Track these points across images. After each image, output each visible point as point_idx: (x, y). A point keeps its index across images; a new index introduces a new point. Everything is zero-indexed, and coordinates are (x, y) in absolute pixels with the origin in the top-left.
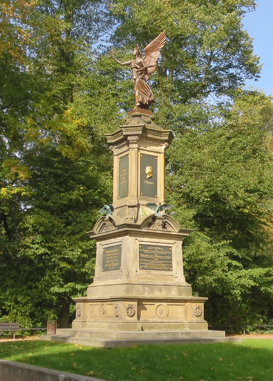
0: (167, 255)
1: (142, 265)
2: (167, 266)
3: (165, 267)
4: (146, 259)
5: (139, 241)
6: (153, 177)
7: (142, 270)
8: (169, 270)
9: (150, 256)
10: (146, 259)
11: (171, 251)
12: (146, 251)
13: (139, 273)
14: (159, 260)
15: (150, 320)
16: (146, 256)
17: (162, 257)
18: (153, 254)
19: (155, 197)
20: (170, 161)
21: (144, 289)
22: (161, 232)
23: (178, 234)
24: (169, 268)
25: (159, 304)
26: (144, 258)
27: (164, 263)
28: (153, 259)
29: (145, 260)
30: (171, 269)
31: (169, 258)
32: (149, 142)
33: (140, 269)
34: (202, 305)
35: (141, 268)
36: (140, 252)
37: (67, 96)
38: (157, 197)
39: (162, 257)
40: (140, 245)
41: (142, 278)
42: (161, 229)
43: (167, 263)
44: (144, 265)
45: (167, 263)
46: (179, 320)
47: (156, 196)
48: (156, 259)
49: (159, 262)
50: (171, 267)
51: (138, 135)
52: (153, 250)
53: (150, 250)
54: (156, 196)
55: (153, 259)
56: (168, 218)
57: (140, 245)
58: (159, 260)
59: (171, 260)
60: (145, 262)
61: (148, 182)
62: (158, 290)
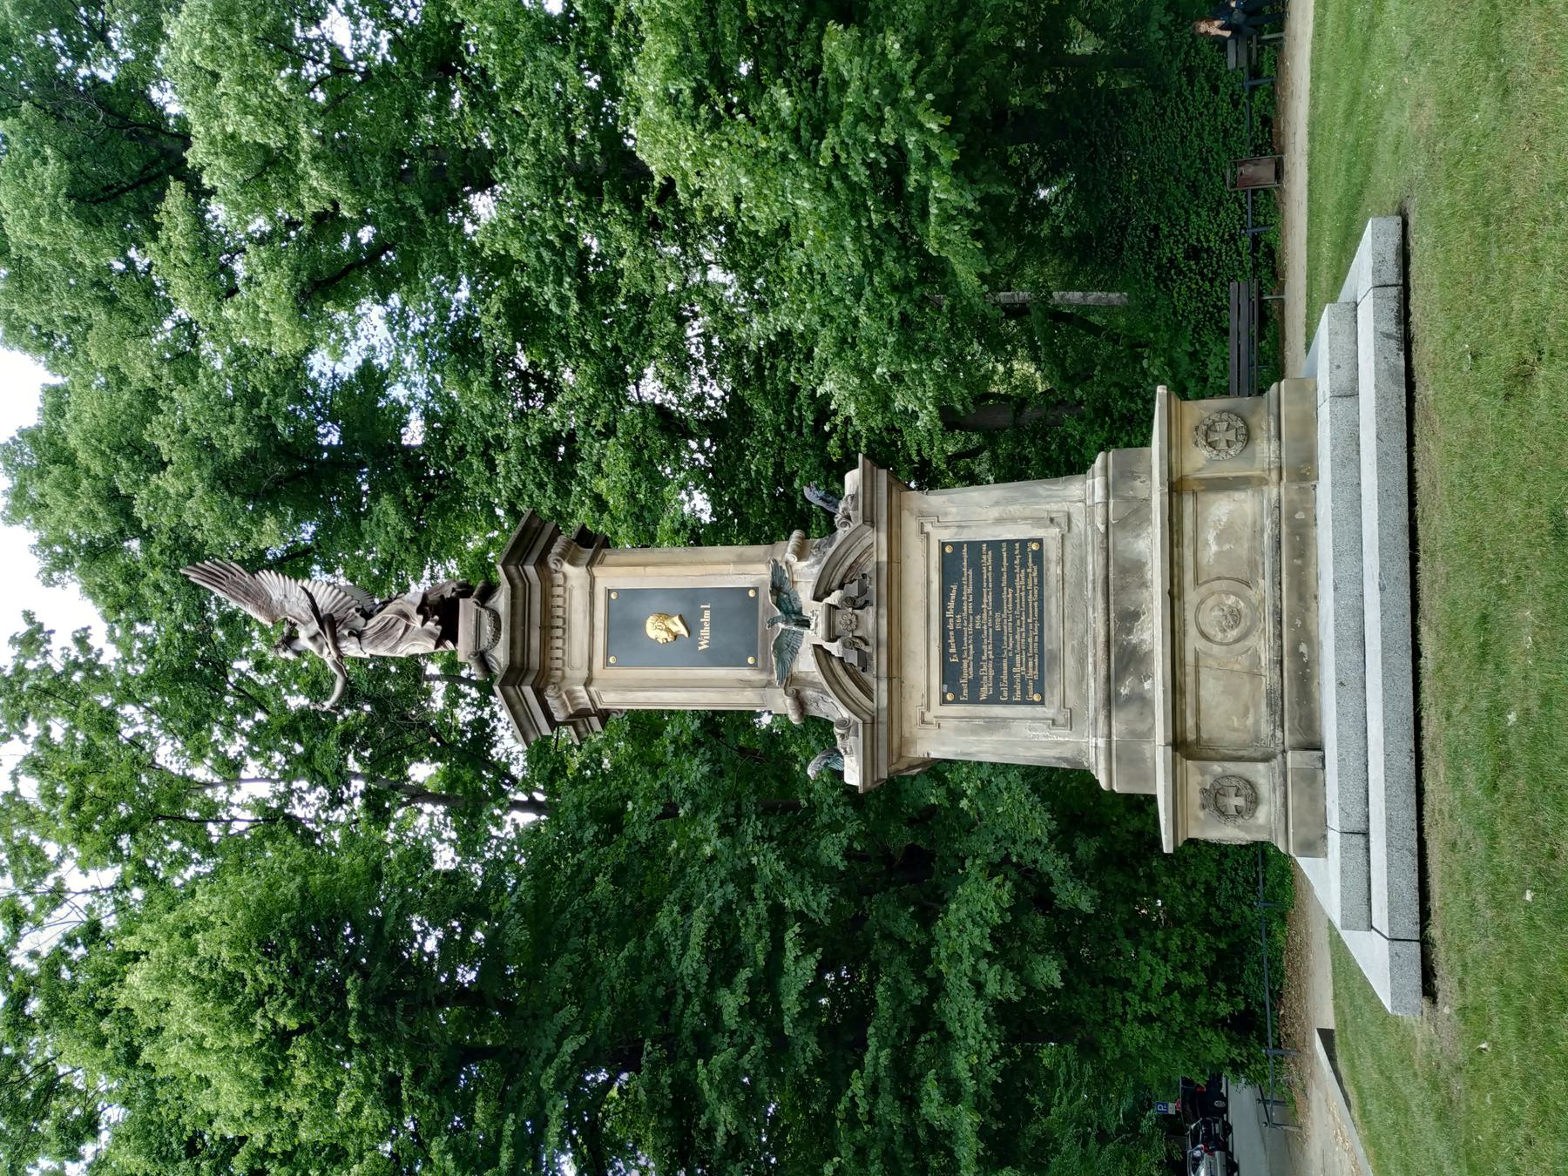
0: (976, 565)
1: (1025, 692)
2: (1024, 565)
3: (1027, 575)
4: (998, 671)
5: (928, 709)
6: (688, 602)
7: (1047, 696)
8: (1039, 557)
9: (988, 652)
10: (998, 671)
11: (958, 546)
12: (967, 671)
13: (1059, 711)
14: (998, 605)
15: (1268, 678)
16: (987, 670)
17: (987, 599)
18: (978, 634)
19: (756, 598)
20: (1099, 1153)
21: (1129, 699)
22: (883, 611)
23: (884, 527)
24: (1027, 554)
25: (1192, 631)
26: (997, 680)
27: (1011, 584)
28: (998, 637)
29: (1005, 677)
30: (1035, 547)
31: (987, 558)
32: (559, 601)
33: (1042, 703)
34: (1198, 410)
35: (1036, 698)
36: (974, 700)
37: (292, 1075)
38: (756, 589)
39: (987, 599)
40: (944, 701)
41: (1084, 698)
42: (871, 610)
43: (1011, 567)
44: (1024, 682)
45: (1011, 567)
46: (1268, 522)
47: (751, 594)
48: (998, 620)
49: (1007, 607)
50: (1024, 543)
51: (539, 694)
52: (959, 634)
53: (960, 653)
54: (751, 594)
55: (998, 637)
56: (842, 551)
57: (944, 701)
58: (998, 605)
59: (995, 545)
60: (1010, 673)
61: (706, 632)
62: (1129, 631)
